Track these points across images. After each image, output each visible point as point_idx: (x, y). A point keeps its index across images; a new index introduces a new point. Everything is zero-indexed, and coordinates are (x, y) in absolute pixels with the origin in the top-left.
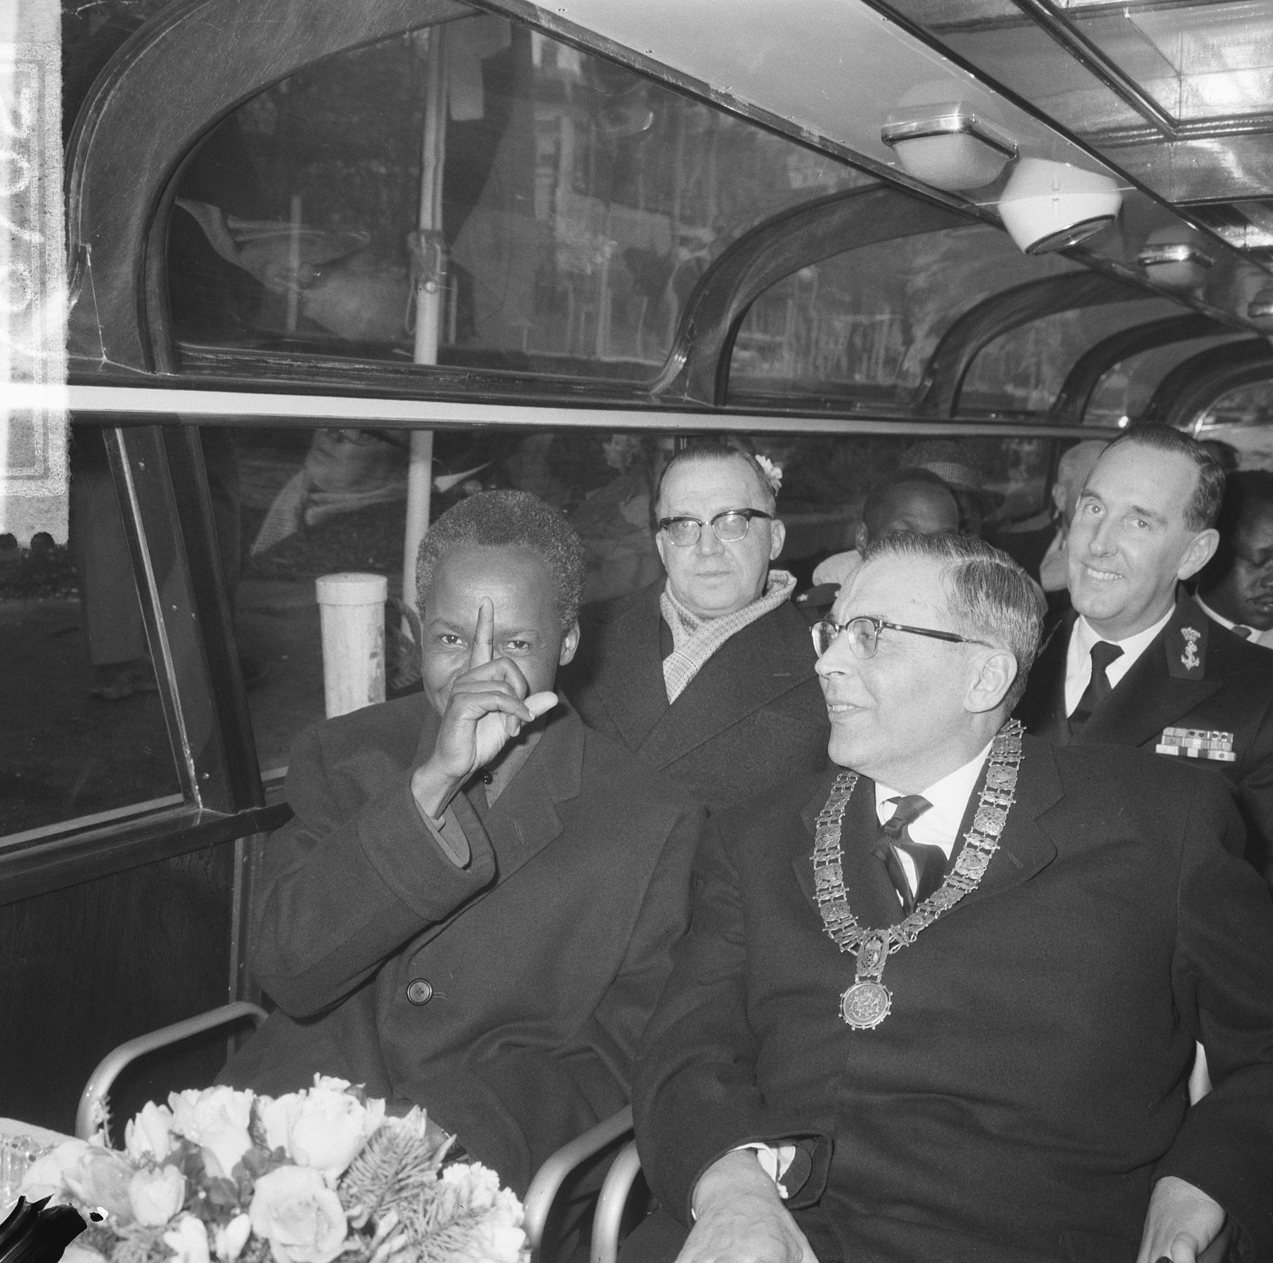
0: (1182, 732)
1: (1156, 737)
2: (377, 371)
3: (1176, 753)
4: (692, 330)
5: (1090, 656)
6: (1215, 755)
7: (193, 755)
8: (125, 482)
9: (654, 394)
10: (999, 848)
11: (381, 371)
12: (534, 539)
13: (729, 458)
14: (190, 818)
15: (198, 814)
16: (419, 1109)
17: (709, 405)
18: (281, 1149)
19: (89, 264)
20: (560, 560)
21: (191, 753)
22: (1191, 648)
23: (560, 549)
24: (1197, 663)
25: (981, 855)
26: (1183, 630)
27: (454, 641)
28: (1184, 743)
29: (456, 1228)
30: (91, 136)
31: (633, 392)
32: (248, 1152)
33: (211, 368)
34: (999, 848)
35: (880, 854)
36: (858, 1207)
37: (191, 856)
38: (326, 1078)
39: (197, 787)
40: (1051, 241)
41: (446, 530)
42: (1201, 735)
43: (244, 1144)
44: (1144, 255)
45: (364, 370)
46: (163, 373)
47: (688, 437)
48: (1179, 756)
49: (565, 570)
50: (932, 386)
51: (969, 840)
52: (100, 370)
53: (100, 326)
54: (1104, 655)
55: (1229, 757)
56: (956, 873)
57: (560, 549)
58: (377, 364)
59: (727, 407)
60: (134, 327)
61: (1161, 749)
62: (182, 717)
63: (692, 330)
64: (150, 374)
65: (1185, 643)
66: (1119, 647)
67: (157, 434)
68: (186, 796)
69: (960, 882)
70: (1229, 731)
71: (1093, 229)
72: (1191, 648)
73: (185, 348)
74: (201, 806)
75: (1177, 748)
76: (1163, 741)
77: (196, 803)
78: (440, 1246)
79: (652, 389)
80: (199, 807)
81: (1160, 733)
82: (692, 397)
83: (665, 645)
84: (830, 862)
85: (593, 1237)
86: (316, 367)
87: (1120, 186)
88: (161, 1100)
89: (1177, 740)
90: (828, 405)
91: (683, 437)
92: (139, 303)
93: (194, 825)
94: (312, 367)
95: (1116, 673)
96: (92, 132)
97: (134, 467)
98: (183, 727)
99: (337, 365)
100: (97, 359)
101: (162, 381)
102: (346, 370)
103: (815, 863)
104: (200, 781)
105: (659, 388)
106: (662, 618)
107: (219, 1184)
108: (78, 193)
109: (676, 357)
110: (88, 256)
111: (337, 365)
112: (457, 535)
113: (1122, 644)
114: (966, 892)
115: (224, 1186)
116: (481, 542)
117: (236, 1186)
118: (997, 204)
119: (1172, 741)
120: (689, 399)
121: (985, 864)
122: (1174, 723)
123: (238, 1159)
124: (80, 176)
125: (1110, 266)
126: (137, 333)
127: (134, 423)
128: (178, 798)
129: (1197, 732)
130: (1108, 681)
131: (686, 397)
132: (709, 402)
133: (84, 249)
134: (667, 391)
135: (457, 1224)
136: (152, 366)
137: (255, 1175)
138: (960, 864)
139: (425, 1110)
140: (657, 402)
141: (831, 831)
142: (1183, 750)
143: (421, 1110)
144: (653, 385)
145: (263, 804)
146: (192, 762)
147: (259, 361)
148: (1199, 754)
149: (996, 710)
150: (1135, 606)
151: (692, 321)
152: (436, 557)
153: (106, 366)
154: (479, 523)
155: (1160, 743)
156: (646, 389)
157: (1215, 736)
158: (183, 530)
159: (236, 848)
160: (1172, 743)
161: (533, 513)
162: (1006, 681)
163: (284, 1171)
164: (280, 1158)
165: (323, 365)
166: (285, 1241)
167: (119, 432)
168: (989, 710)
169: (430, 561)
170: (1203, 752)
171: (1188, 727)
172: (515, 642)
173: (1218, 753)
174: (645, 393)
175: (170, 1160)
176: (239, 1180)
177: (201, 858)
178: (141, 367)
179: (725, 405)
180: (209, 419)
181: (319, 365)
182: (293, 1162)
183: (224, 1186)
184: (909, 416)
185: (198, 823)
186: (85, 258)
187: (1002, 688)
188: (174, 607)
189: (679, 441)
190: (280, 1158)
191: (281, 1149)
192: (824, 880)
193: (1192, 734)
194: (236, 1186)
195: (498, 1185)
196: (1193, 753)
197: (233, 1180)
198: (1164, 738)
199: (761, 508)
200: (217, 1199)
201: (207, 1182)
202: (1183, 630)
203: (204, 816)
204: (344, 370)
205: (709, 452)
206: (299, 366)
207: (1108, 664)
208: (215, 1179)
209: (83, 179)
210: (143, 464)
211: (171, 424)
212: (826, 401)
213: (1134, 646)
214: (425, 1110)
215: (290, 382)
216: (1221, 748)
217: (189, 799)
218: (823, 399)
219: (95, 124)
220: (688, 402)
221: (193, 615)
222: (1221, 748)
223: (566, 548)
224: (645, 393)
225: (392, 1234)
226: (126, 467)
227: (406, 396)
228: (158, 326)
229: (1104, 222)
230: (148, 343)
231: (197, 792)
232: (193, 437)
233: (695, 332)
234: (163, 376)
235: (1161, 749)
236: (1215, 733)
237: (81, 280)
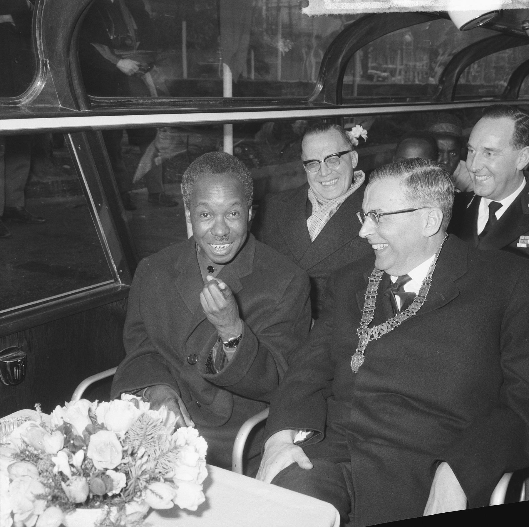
1: (517, 240)
2: (181, 101)
4: (325, 73)
5: (488, 208)
7: (115, 263)
8: (75, 155)
9: (310, 102)
11: (183, 101)
12: (234, 170)
13: (329, 131)
14: (118, 288)
15: (120, 286)
16: (165, 406)
17: (334, 105)
18: (103, 424)
19: (49, 67)
21: (114, 262)
27: (206, 216)
29: (170, 453)
30: (41, 15)
31: (300, 102)
32: (89, 425)
33: (107, 106)
35: (387, 295)
36: (361, 439)
37: (117, 303)
39: (118, 276)
40: (472, 23)
41: (196, 170)
43: (87, 422)
44: (524, 25)
45: (176, 101)
46: (84, 110)
47: (326, 119)
48: (527, 248)
50: (443, 88)
52: (59, 110)
53: (57, 93)
54: (494, 207)
58: (181, 99)
59: (343, 105)
61: (519, 245)
62: (109, 248)
63: (325, 73)
64: (78, 111)
66: (500, 203)
67: (83, 135)
68: (115, 280)
71: (490, 17)
73: (91, 98)
74: (121, 283)
76: (520, 242)
77: (118, 281)
78: (165, 460)
79: (309, 100)
80: (120, 284)
81: (519, 238)
82: (327, 102)
83: (308, 210)
84: (372, 297)
86: (154, 102)
88: (63, 405)
89: (526, 241)
90: (393, 100)
91: (324, 119)
92: (69, 82)
93: (118, 290)
94: (152, 102)
95: (499, 214)
96: (41, 13)
98: (110, 252)
99: (163, 100)
100: (57, 106)
101: (83, 113)
102: (168, 102)
103: (366, 297)
104: (119, 273)
105: (312, 99)
106: (308, 199)
107: (77, 438)
108: (40, 38)
109: (319, 86)
110: (48, 64)
111: (163, 100)
112: (202, 171)
113: (502, 202)
115: (79, 439)
116: (213, 173)
117: (84, 439)
119: (523, 241)
120: (326, 103)
123: (84, 428)
124: (40, 31)
125: (512, 31)
126: (70, 94)
127: (75, 131)
128: (113, 281)
130: (496, 217)
131: (325, 102)
133: (46, 61)
134: (316, 100)
135: (171, 452)
136: (78, 108)
137: (90, 434)
139: (167, 407)
140: (312, 105)
141: (375, 285)
143: (166, 407)
144: (309, 98)
146: (115, 266)
147: (128, 101)
149: (439, 232)
150: (500, 187)
151: (325, 69)
152: (193, 182)
153: (61, 109)
154: (211, 165)
155: (518, 243)
156: (306, 100)
158: (99, 174)
160: (523, 243)
162: (439, 222)
163: (101, 432)
164: (103, 427)
165: (157, 101)
166: (23, 474)
167: (69, 135)
168: (435, 234)
169: (191, 184)
172: (232, 213)
174: (306, 102)
175: (59, 429)
176: (85, 436)
177: (121, 304)
178: (73, 108)
179: (342, 104)
180: (105, 127)
181: (155, 101)
182: (106, 429)
183: (79, 439)
184: (433, 102)
185: (120, 290)
186: (47, 65)
187: (438, 223)
188: (100, 204)
190: (103, 427)
191: (103, 424)
192: (368, 304)
194: (84, 439)
195: (198, 435)
197: (82, 436)
198: (520, 240)
199: (346, 149)
200: (77, 444)
201: (74, 437)
203: (122, 287)
204: (166, 102)
205: (319, 129)
206: (147, 102)
207: (496, 211)
208: (76, 436)
209: (41, 33)
210: (80, 148)
211: (89, 131)
212: (392, 98)
213: (507, 202)
214: (167, 407)
215: (144, 109)
217: (116, 280)
218: (390, 98)
219: (42, 10)
220: (325, 104)
221: (107, 207)
224: (306, 102)
225: (144, 456)
226: (74, 149)
227: (193, 112)
228: (79, 91)
229: (495, 13)
230: (76, 99)
232: (99, 135)
233: (326, 74)
234: (83, 111)
237: (46, 74)
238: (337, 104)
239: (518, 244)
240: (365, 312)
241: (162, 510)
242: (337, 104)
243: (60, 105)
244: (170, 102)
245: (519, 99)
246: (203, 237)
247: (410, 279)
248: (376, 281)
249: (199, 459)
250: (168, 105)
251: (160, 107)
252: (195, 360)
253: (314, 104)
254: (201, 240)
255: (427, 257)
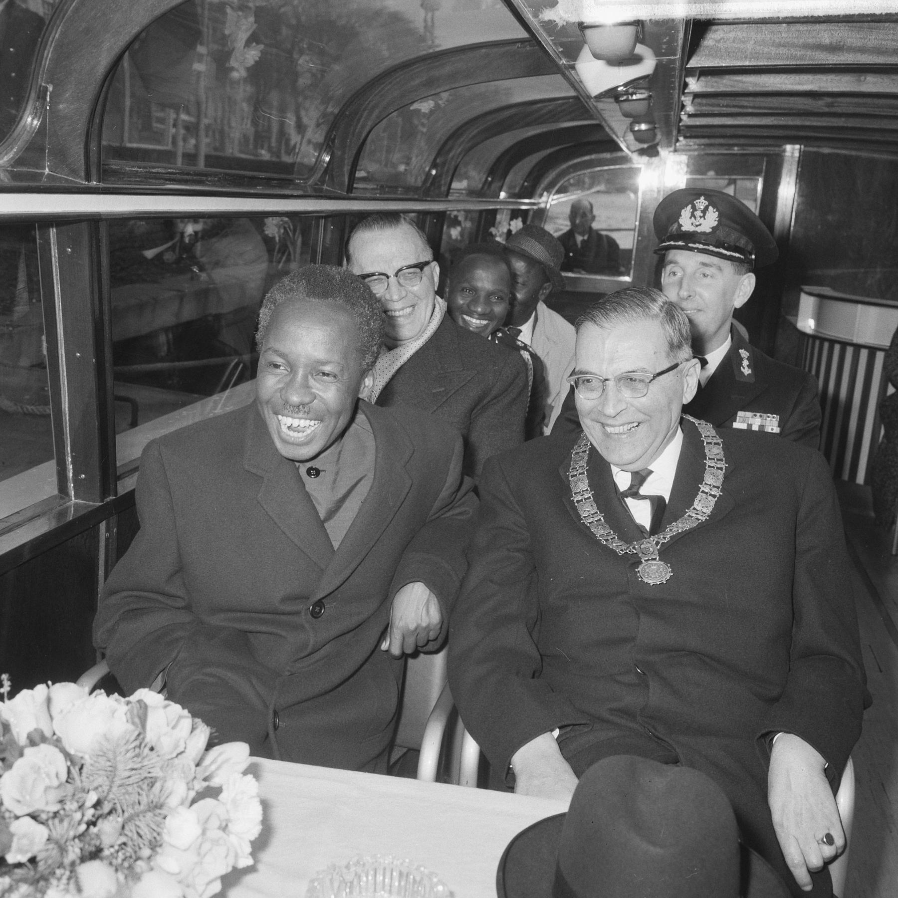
0: (749, 414)
3: (746, 428)
6: (768, 429)
9: (309, 185)
10: (721, 494)
20: (366, 316)
22: (745, 363)
23: (366, 309)
24: (750, 372)
25: (710, 498)
26: (740, 351)
28: (751, 421)
34: (721, 494)
38: (58, 685)
42: (761, 416)
49: (368, 324)
51: (702, 489)
55: (776, 430)
56: (694, 509)
57: (366, 309)
60: (80, 148)
61: (736, 425)
64: (87, 183)
65: (742, 359)
69: (697, 514)
70: (777, 415)
72: (745, 363)
74: (73, 498)
75: (746, 425)
85: (420, 761)
87: (656, 57)
97: (61, 252)
114: (700, 521)
118: (574, 64)
121: (713, 504)
122: (744, 409)
129: (758, 414)
132: (344, 191)
138: (697, 503)
142: (750, 425)
145: (116, 494)
148: (759, 428)
157: (768, 417)
159: (101, 528)
160: (744, 422)
161: (350, 281)
170: (761, 426)
171: (752, 412)
173: (771, 428)
186: (46, 95)
189: (319, 222)
193: (755, 415)
196: (755, 428)
198: (738, 418)
202: (740, 351)
203: (76, 504)
211: (93, 220)
216: (772, 424)
221: (94, 361)
222: (772, 424)
223: (371, 310)
226: (54, 252)
231: (72, 488)
235: (736, 425)
236: (769, 415)
238: (88, 178)
239: (734, 423)
240: (689, 516)
241: (832, 789)
242: (88, 178)
243: (47, 170)
244: (167, 173)
245: (450, 198)
246: (268, 401)
247: (651, 472)
248: (580, 474)
249: (48, 840)
250: (163, 179)
251: (153, 181)
252: (320, 610)
253: (315, 190)
254: (265, 406)
255: (667, 439)
